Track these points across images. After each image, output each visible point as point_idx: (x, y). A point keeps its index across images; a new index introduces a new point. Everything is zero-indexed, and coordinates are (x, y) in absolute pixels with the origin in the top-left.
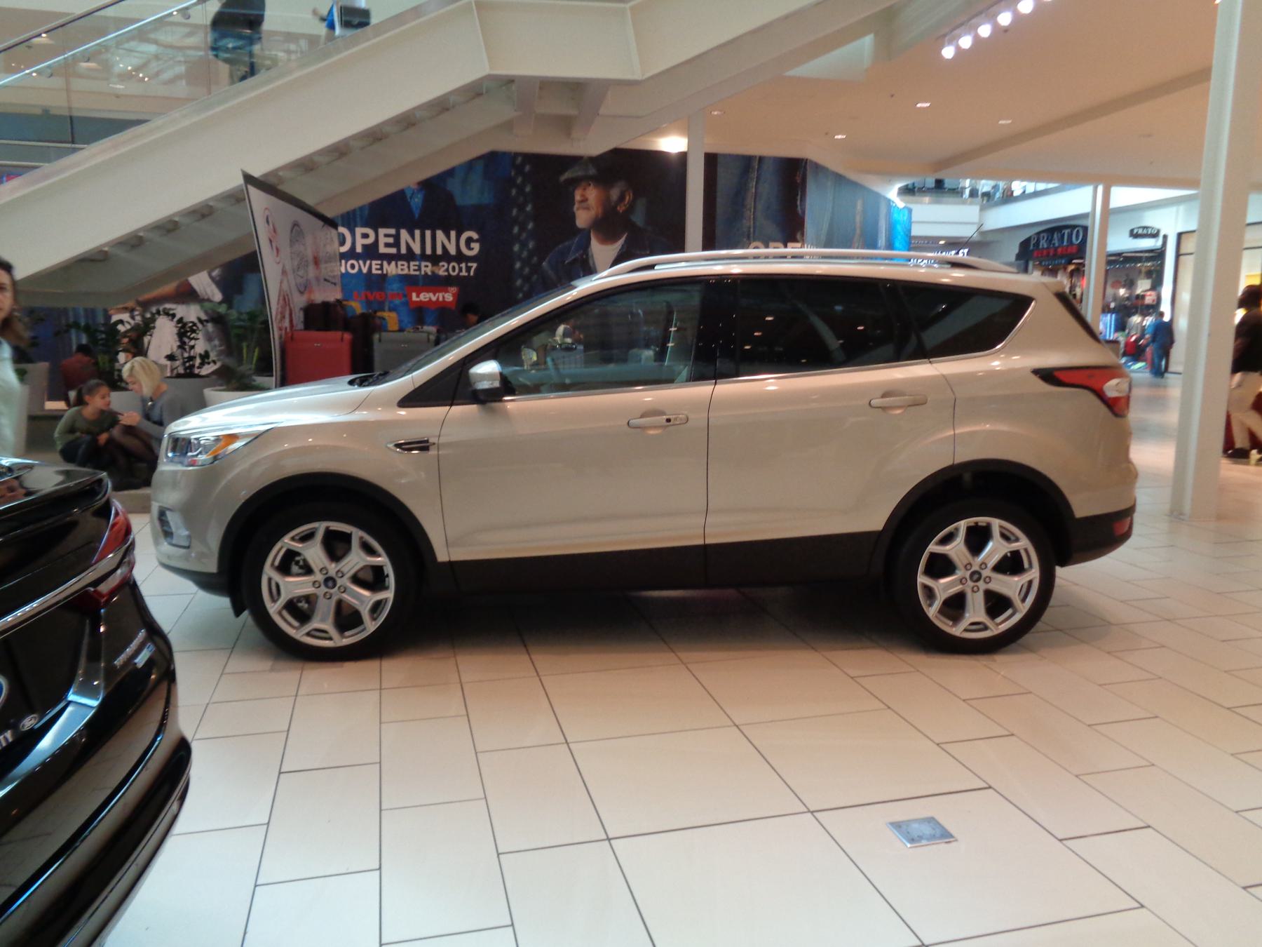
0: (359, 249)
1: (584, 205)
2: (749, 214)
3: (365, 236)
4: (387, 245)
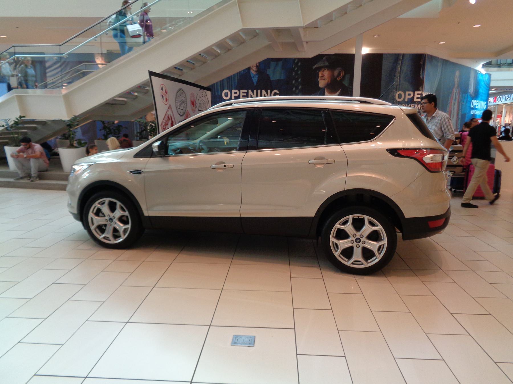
0: (406, 100)
1: (323, 78)
2: (397, 79)
3: (235, 93)
4: (418, 98)
